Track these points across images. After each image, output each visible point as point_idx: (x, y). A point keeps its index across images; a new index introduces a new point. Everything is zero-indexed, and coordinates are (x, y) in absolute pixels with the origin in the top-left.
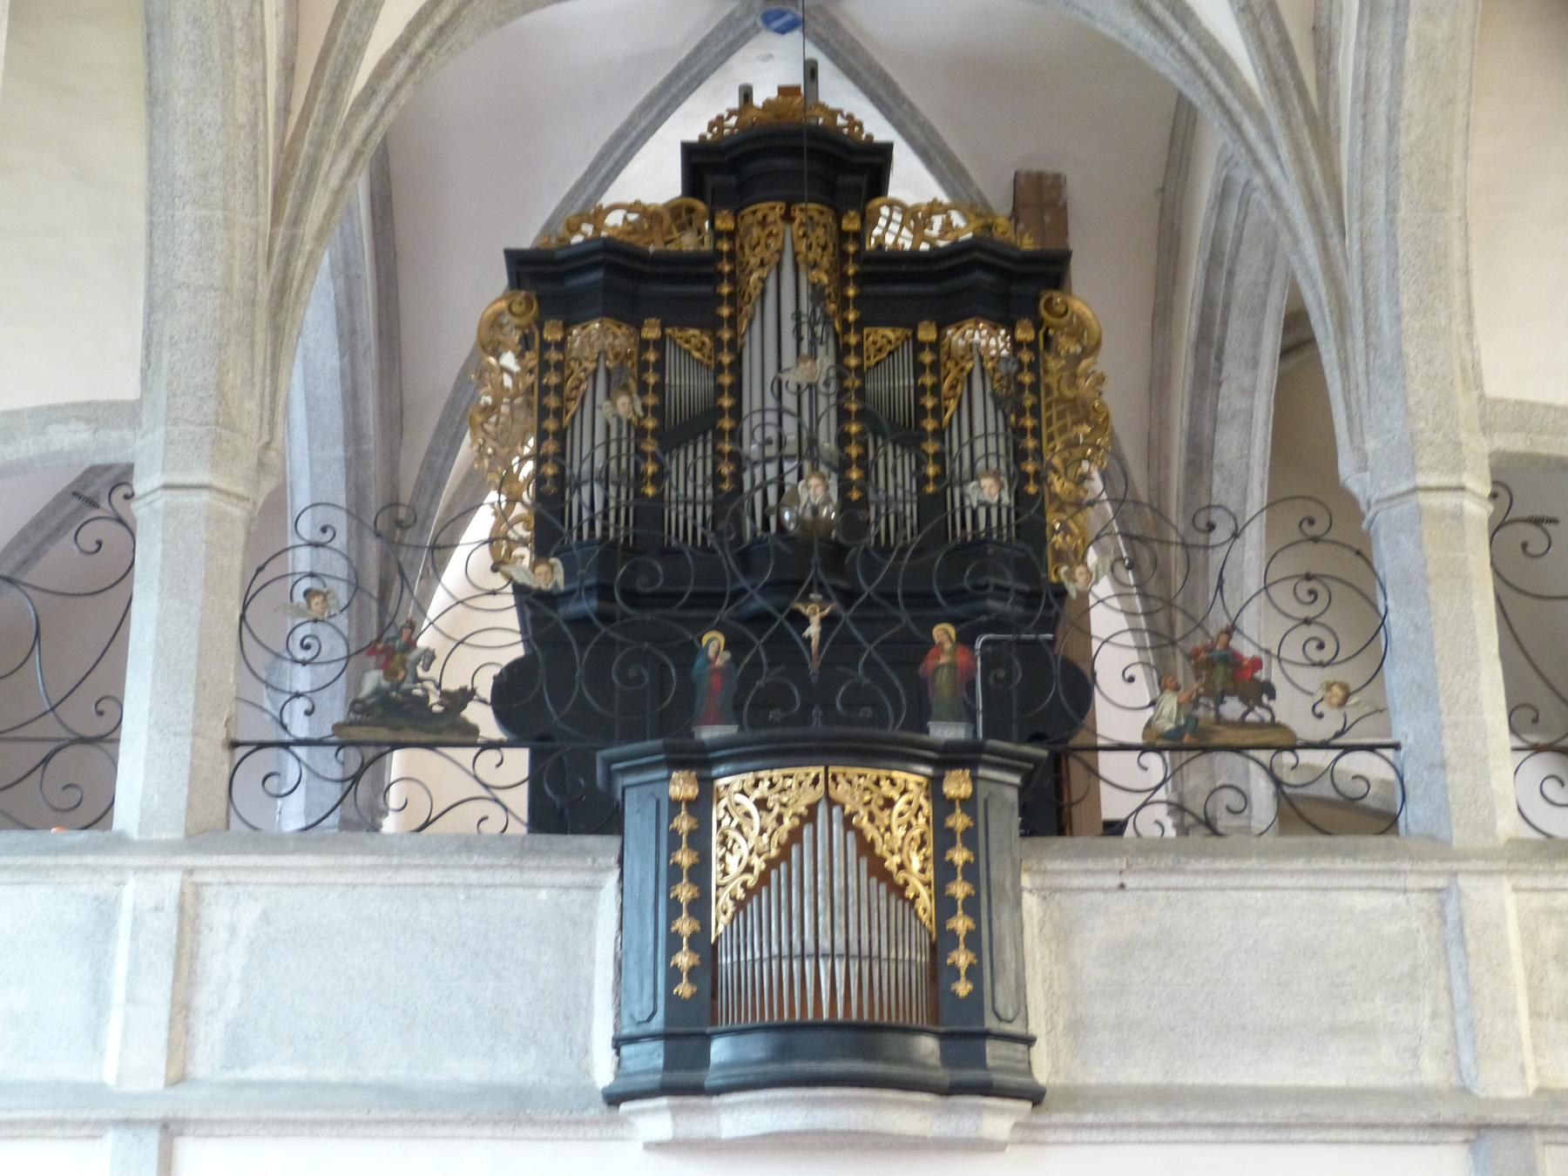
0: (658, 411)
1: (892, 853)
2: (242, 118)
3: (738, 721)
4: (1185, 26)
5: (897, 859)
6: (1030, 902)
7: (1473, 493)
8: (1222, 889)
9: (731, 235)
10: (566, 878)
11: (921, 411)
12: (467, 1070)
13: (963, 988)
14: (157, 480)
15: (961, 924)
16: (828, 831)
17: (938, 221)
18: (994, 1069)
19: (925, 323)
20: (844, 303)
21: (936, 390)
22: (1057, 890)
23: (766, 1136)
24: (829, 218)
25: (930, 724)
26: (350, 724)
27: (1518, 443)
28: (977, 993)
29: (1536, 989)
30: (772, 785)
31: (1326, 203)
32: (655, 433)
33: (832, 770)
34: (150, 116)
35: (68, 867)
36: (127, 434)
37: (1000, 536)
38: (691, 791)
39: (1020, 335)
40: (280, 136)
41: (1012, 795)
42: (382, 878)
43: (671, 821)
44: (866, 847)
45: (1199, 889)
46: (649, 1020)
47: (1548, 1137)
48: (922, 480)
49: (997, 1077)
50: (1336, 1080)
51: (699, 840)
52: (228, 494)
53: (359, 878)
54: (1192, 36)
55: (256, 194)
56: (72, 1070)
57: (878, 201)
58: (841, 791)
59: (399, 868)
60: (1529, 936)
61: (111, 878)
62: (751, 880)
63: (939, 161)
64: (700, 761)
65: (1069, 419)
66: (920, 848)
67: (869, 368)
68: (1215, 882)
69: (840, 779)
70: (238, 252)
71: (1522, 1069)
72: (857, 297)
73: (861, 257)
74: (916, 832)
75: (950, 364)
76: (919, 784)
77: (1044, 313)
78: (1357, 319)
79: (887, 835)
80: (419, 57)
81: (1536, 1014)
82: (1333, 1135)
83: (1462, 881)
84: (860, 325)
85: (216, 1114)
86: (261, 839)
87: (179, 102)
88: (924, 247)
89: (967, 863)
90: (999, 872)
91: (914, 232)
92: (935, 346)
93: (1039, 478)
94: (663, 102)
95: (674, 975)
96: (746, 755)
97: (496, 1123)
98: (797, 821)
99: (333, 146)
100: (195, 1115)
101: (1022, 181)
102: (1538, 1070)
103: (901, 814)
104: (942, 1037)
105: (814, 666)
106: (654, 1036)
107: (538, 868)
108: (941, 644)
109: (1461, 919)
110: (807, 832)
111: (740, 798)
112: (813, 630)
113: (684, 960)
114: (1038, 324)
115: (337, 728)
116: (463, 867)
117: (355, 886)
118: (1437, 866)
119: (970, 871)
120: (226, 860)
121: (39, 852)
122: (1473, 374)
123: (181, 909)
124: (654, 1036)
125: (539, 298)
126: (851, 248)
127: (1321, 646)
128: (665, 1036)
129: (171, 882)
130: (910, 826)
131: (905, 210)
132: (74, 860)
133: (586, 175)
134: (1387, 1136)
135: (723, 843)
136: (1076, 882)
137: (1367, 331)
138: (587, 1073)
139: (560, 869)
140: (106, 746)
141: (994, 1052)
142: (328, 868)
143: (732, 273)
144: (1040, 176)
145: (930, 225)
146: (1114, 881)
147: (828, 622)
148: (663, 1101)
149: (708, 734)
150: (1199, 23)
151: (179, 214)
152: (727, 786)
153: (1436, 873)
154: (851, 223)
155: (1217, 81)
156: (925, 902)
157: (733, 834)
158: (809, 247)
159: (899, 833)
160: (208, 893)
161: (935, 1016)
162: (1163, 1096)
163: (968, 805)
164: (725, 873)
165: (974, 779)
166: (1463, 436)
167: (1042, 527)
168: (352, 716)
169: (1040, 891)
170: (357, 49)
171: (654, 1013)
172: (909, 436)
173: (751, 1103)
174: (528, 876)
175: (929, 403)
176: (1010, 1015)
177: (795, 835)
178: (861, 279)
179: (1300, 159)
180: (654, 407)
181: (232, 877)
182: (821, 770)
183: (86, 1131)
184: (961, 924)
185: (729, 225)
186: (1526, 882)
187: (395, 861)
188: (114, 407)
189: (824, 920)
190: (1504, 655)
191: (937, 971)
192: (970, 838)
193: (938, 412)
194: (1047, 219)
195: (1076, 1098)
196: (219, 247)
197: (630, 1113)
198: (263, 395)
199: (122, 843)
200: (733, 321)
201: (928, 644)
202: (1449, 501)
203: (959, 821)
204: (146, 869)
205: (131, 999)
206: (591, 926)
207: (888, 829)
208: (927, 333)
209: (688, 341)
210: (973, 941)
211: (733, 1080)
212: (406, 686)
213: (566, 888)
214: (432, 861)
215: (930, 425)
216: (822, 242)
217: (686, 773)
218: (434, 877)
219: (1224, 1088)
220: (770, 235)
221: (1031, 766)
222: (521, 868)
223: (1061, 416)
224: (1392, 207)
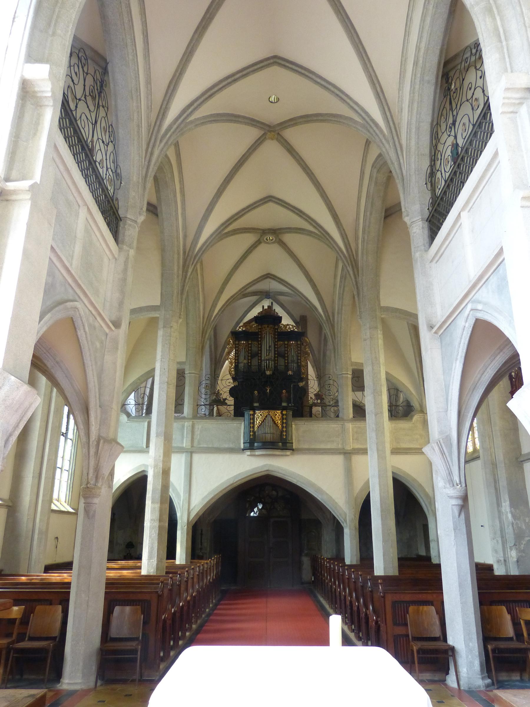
0: (251, 353)
6: (293, 426)
9: (260, 329)
10: (238, 423)
12: (226, 446)
13: (284, 437)
14: (188, 372)
15: (284, 429)
16: (269, 418)
20: (275, 338)
27: (356, 367)
29: (353, 436)
38: (253, 413)
39: (298, 343)
40: (202, 327)
41: (291, 413)
44: (273, 420)
48: (285, 363)
51: (253, 419)
56: (180, 445)
60: (353, 430)
64: (254, 409)
81: (353, 439)
84: (277, 341)
90: (289, 423)
92: (287, 344)
93: (300, 362)
95: (250, 435)
96: (261, 408)
112: (268, 391)
114: (301, 341)
119: (286, 423)
122: (350, 359)
129: (191, 423)
141: (288, 445)
144: (303, 316)
146: (303, 423)
147: (269, 390)
149: (256, 405)
154: (276, 327)
163: (286, 415)
169: (295, 425)
172: (283, 356)
177: (265, 419)
184: (284, 429)
186: (353, 423)
189: (268, 429)
191: (281, 435)
192: (286, 419)
193: (287, 353)
202: (346, 375)
203: (285, 417)
205: (187, 437)
206: (241, 428)
208: (286, 343)
210: (286, 431)
215: (286, 355)
224: (340, 338)
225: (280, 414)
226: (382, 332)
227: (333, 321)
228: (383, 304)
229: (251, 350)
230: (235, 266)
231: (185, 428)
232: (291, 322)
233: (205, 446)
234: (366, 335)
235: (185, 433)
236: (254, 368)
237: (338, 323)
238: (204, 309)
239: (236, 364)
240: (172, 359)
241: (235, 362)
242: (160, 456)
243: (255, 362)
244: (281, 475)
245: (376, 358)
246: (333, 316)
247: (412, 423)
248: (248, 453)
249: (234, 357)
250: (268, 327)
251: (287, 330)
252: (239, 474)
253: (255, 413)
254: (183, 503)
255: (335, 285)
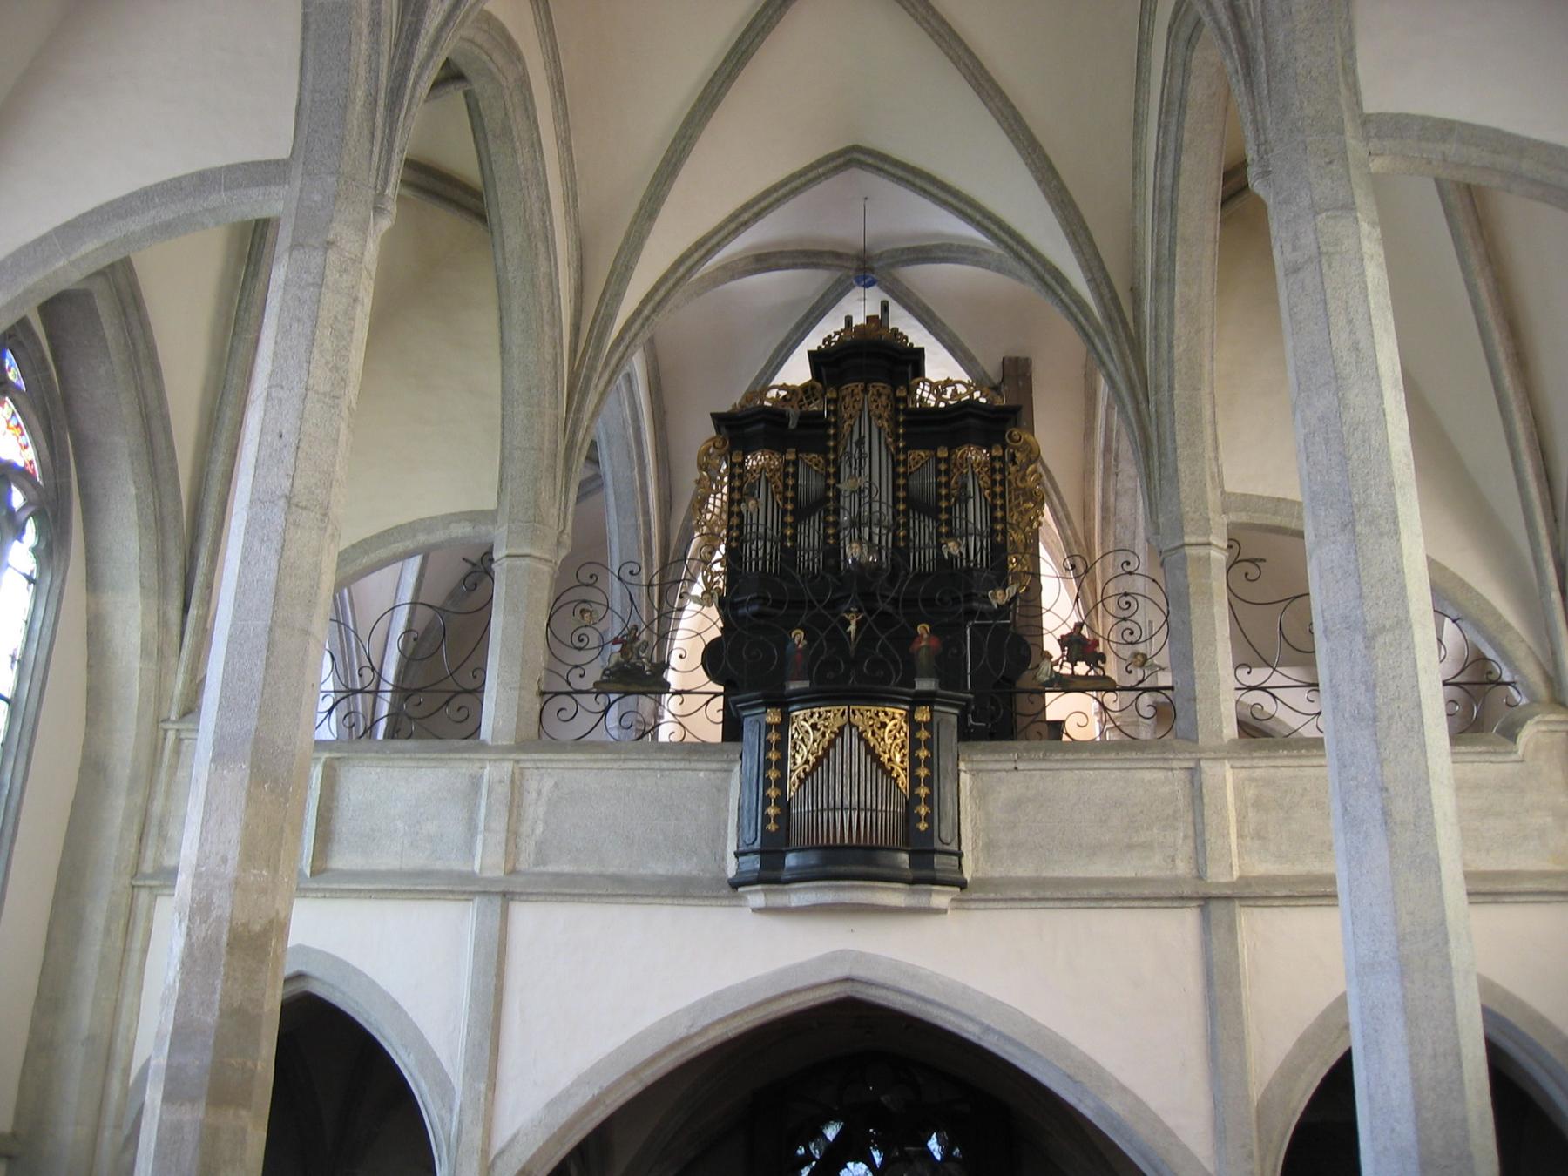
1: (885, 752)
2: (548, 358)
3: (811, 679)
4: (1063, 289)
5: (887, 756)
7: (1216, 546)
8: (1071, 769)
9: (835, 401)
10: (714, 766)
11: (939, 497)
12: (660, 868)
13: (923, 826)
15: (923, 791)
16: (850, 741)
17: (949, 390)
18: (939, 871)
19: (942, 447)
20: (897, 438)
21: (947, 484)
22: (981, 771)
23: (815, 906)
24: (888, 390)
25: (916, 679)
26: (602, 682)
27: (1243, 518)
28: (930, 830)
29: (1241, 821)
30: (820, 716)
31: (1138, 385)
32: (792, 513)
33: (852, 707)
34: (502, 358)
35: (455, 759)
36: (490, 528)
37: (975, 565)
40: (571, 364)
41: (954, 719)
42: (616, 765)
43: (766, 735)
44: (870, 750)
45: (1058, 770)
46: (753, 843)
47: (1244, 903)
49: (939, 875)
50: (1130, 874)
51: (782, 746)
52: (540, 559)
53: (604, 765)
54: (1067, 294)
55: (557, 397)
56: (457, 865)
57: (917, 380)
58: (857, 719)
59: (625, 760)
60: (1239, 791)
61: (478, 764)
62: (808, 768)
63: (960, 354)
64: (783, 703)
65: (1021, 499)
66: (901, 750)
67: (911, 473)
68: (1066, 766)
69: (857, 712)
70: (547, 429)
71: (1231, 866)
72: (904, 434)
73: (906, 411)
74: (899, 741)
75: (955, 470)
76: (901, 714)
77: (1008, 440)
78: (1155, 449)
79: (882, 743)
80: (648, 318)
81: (1240, 836)
82: (1126, 904)
83: (1203, 763)
84: (905, 449)
85: (529, 890)
86: (556, 745)
87: (515, 351)
88: (942, 405)
89: (926, 757)
90: (946, 763)
91: (935, 396)
92: (947, 460)
93: (1004, 532)
94: (805, 326)
95: (766, 819)
96: (809, 699)
97: (674, 897)
98: (833, 736)
99: (599, 369)
100: (518, 890)
101: (1007, 363)
102: (1240, 867)
103: (890, 731)
104: (911, 853)
105: (852, 648)
106: (755, 852)
107: (698, 761)
108: (922, 635)
109: (1201, 784)
110: (839, 741)
111: (803, 723)
112: (852, 628)
113: (772, 811)
115: (596, 684)
116: (659, 760)
117: (603, 769)
118: (1188, 756)
119: (929, 763)
120: (535, 756)
121: (441, 751)
123: (512, 781)
124: (755, 852)
125: (731, 439)
126: (901, 407)
127: (1132, 633)
128: (760, 852)
129: (508, 767)
130: (895, 737)
131: (931, 384)
132: (458, 756)
133: (765, 366)
134: (1156, 904)
135: (794, 747)
136: (990, 766)
137: (1159, 457)
138: (724, 870)
139: (710, 761)
140: (477, 694)
141: (938, 860)
142: (587, 760)
143: (836, 422)
144: (1017, 359)
145: (945, 393)
146: (1011, 766)
147: (858, 623)
148: (759, 887)
150: (1070, 286)
151: (516, 410)
152: (797, 716)
153: (1188, 759)
154: (901, 393)
155: (1081, 318)
156: (903, 780)
157: (799, 743)
158: (877, 407)
159: (889, 742)
160: (527, 773)
161: (907, 843)
162: (1037, 883)
163: (928, 726)
164: (795, 764)
165: (931, 711)
166: (1211, 515)
167: (1005, 564)
168: (605, 678)
169: (974, 773)
170: (611, 318)
171: (756, 839)
173: (805, 888)
174: (693, 765)
175: (943, 492)
176: (949, 841)
177: (832, 743)
178: (906, 424)
179: (1124, 362)
180: (792, 498)
181: (539, 765)
182: (846, 708)
183: (465, 897)
184: (923, 791)
185: (834, 395)
186: (1238, 764)
187: (623, 756)
188: (483, 513)
189: (847, 789)
190: (1232, 637)
191: (909, 817)
192: (929, 744)
194: (1021, 383)
195: (984, 883)
196: (536, 427)
197: (743, 892)
198: (560, 505)
199: (483, 747)
200: (835, 449)
201: (915, 636)
202: (1202, 551)
203: (923, 735)
204: (495, 760)
205: (487, 829)
206: (727, 791)
207: (883, 739)
208: (942, 453)
209: (811, 461)
210: (929, 800)
211: (794, 877)
212: (633, 661)
213: (714, 771)
214: (642, 757)
216: (884, 404)
217: (774, 710)
218: (644, 765)
219: (1068, 878)
220: (856, 400)
221: (964, 704)
222: (690, 761)
223: (1017, 498)
224: (1171, 388)
225: (899, 720)
226: (1377, 233)
227: (1138, 332)
228: (1371, 106)
229: (795, 487)
230: (701, 99)
231: (484, 791)
232: (958, 373)
233: (568, 868)
234: (1294, 249)
235: (483, 811)
236: (810, 558)
237: (1156, 328)
238: (580, 291)
239: (734, 544)
240: (322, 389)
241: (729, 539)
242: (225, 860)
243: (810, 535)
244: (911, 1001)
245: (1356, 348)
246: (1135, 293)
247: (1513, 757)
248: (756, 897)
249: (724, 517)
250: (865, 391)
251: (945, 401)
252: (716, 997)
253: (786, 721)
254: (460, 1122)
255: (1137, 167)
